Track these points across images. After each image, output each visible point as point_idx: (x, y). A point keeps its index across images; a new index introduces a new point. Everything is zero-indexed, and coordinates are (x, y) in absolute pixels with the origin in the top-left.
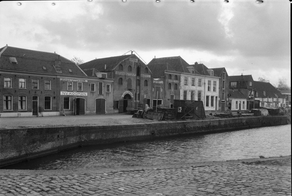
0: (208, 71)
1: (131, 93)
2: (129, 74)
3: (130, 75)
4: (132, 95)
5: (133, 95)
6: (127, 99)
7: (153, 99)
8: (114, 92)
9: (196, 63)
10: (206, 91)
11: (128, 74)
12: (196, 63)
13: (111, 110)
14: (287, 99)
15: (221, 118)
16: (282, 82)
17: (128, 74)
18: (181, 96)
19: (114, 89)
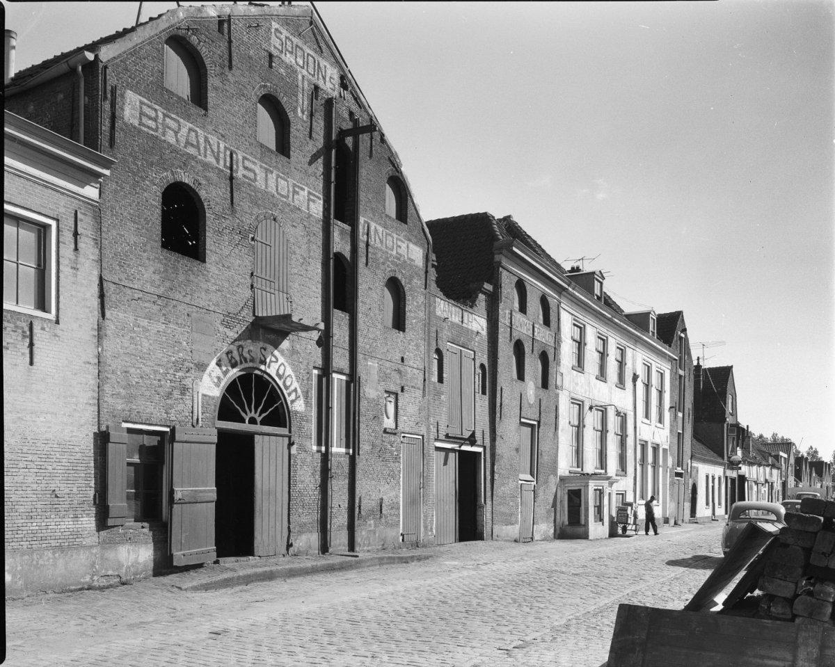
0: (5, 114)
1: (289, 371)
2: (267, 171)
3: (272, 189)
4: (296, 385)
5: (306, 396)
6: (253, 421)
7: (437, 440)
8: (110, 327)
9: (62, 53)
10: (632, 413)
11: (261, 175)
12: (62, 53)
13: (68, 546)
14: (394, 430)
15: (765, 624)
16: (185, 262)
17: (261, 175)
18: (562, 430)
19: (110, 289)
